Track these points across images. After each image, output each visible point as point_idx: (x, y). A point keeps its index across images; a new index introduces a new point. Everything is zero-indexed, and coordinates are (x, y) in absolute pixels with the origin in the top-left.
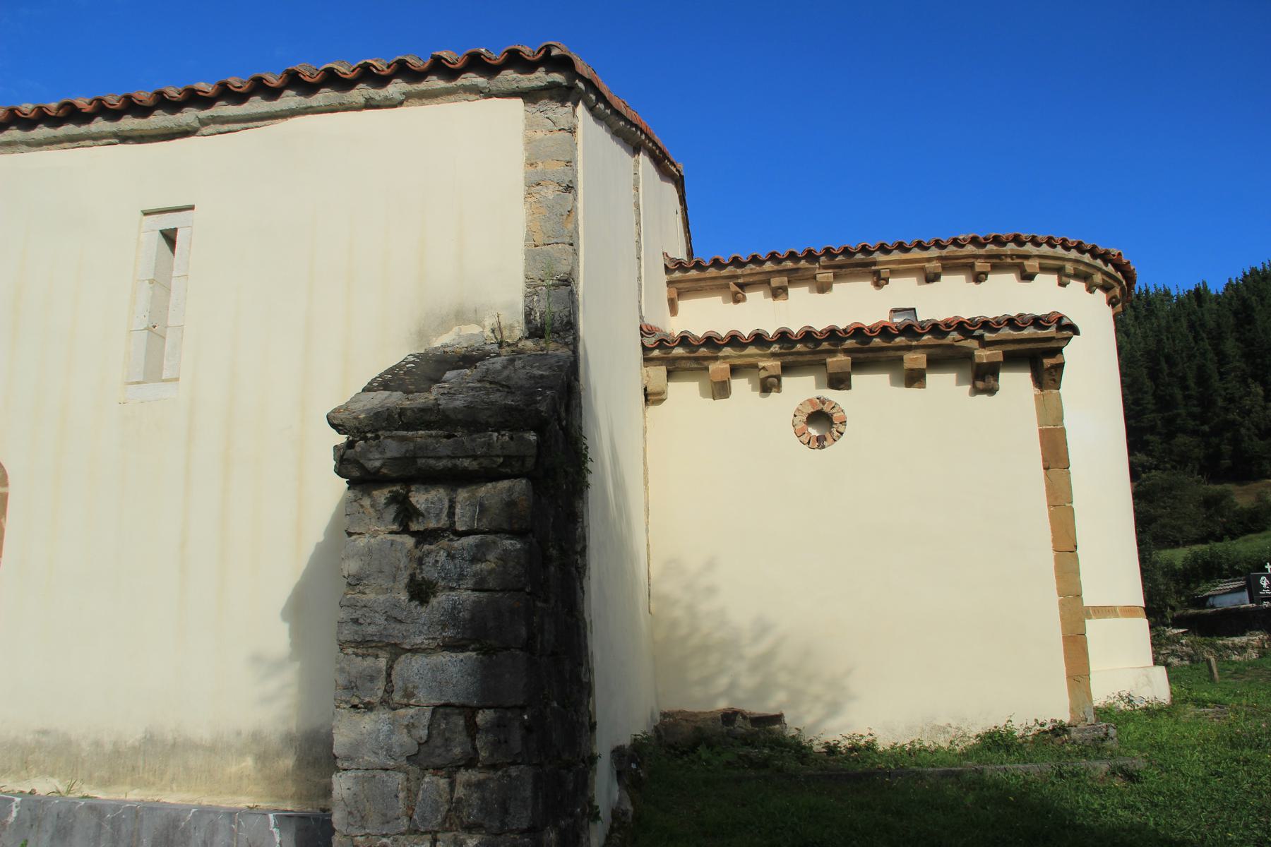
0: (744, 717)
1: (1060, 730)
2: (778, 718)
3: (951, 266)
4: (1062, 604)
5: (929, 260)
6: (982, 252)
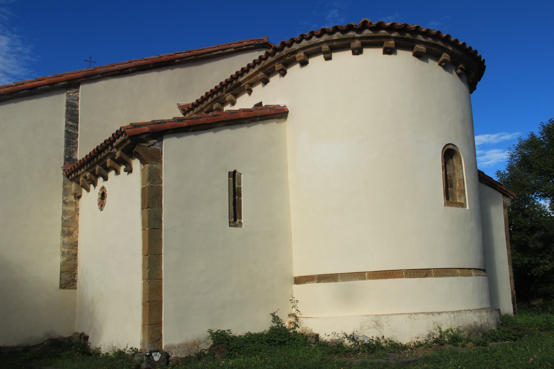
5: (257, 73)
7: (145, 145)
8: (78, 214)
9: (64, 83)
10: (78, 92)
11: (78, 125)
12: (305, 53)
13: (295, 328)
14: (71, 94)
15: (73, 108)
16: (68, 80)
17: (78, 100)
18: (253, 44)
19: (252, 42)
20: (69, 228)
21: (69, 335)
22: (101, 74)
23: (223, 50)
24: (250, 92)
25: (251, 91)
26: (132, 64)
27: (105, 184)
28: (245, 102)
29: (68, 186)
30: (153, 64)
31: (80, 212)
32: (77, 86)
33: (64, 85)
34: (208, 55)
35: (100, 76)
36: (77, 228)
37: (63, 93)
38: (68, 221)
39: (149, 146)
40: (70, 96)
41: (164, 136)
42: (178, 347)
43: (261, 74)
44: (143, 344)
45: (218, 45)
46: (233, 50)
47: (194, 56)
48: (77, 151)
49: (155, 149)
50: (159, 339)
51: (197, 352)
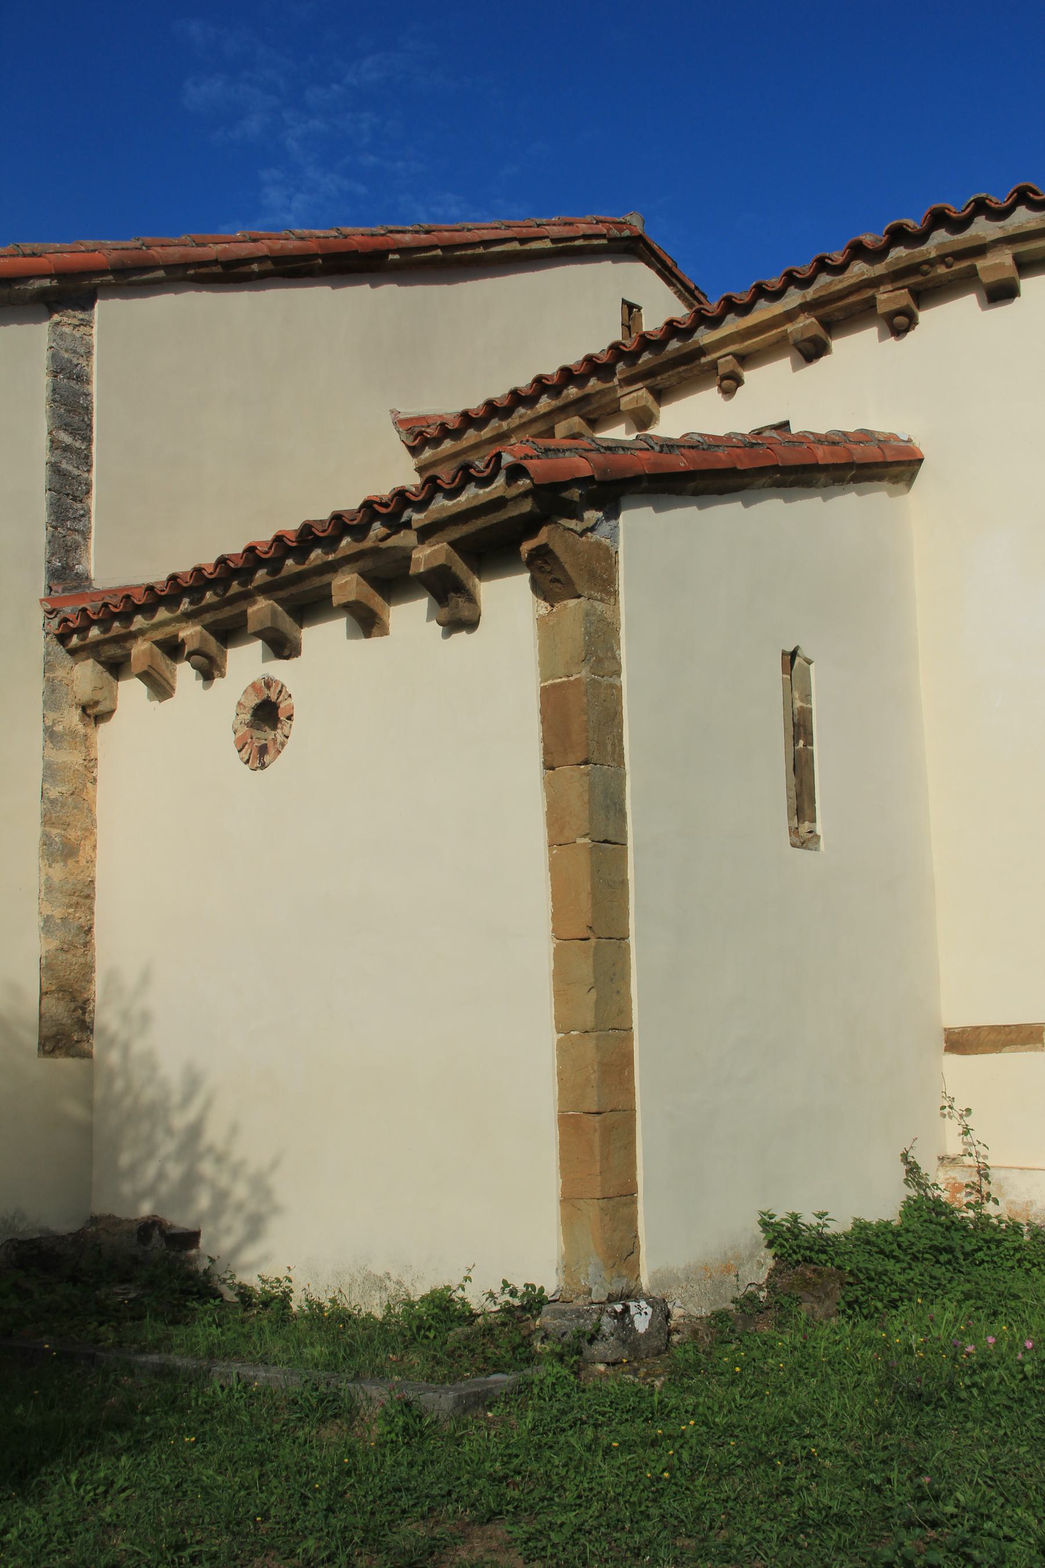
0: (162, 1232)
1: (534, 1302)
2: (191, 1238)
3: (840, 316)
4: (563, 1050)
5: (789, 316)
6: (880, 269)
7: (572, 524)
8: (94, 781)
9: (47, 283)
10: (87, 323)
11: (89, 447)
12: (1015, 257)
13: (979, 1205)
14: (67, 330)
15: (73, 383)
16: (61, 275)
17: (89, 353)
18: (603, 236)
19: (602, 229)
20: (67, 829)
21: (74, 1227)
22: (167, 267)
23: (523, 241)
24: (730, 384)
25: (739, 382)
26: (262, 248)
27: (280, 670)
28: (693, 416)
29: (60, 673)
30: (326, 257)
31: (100, 772)
32: (86, 303)
33: (43, 292)
34: (481, 250)
35: (161, 273)
36: (92, 833)
37: (38, 321)
38: (63, 805)
39: (582, 534)
40: (62, 335)
41: (624, 500)
42: (687, 1279)
43: (806, 324)
44: (568, 1268)
45: (511, 222)
46: (547, 244)
47: (443, 248)
48: (87, 546)
49: (598, 545)
50: (623, 1253)
51: (738, 1295)
